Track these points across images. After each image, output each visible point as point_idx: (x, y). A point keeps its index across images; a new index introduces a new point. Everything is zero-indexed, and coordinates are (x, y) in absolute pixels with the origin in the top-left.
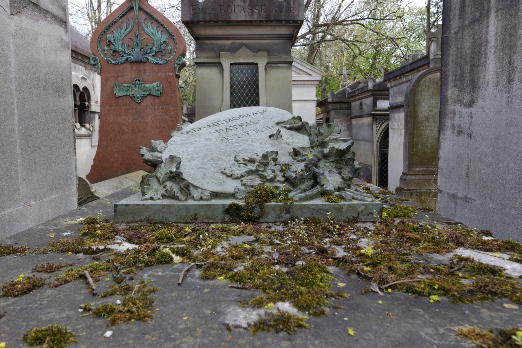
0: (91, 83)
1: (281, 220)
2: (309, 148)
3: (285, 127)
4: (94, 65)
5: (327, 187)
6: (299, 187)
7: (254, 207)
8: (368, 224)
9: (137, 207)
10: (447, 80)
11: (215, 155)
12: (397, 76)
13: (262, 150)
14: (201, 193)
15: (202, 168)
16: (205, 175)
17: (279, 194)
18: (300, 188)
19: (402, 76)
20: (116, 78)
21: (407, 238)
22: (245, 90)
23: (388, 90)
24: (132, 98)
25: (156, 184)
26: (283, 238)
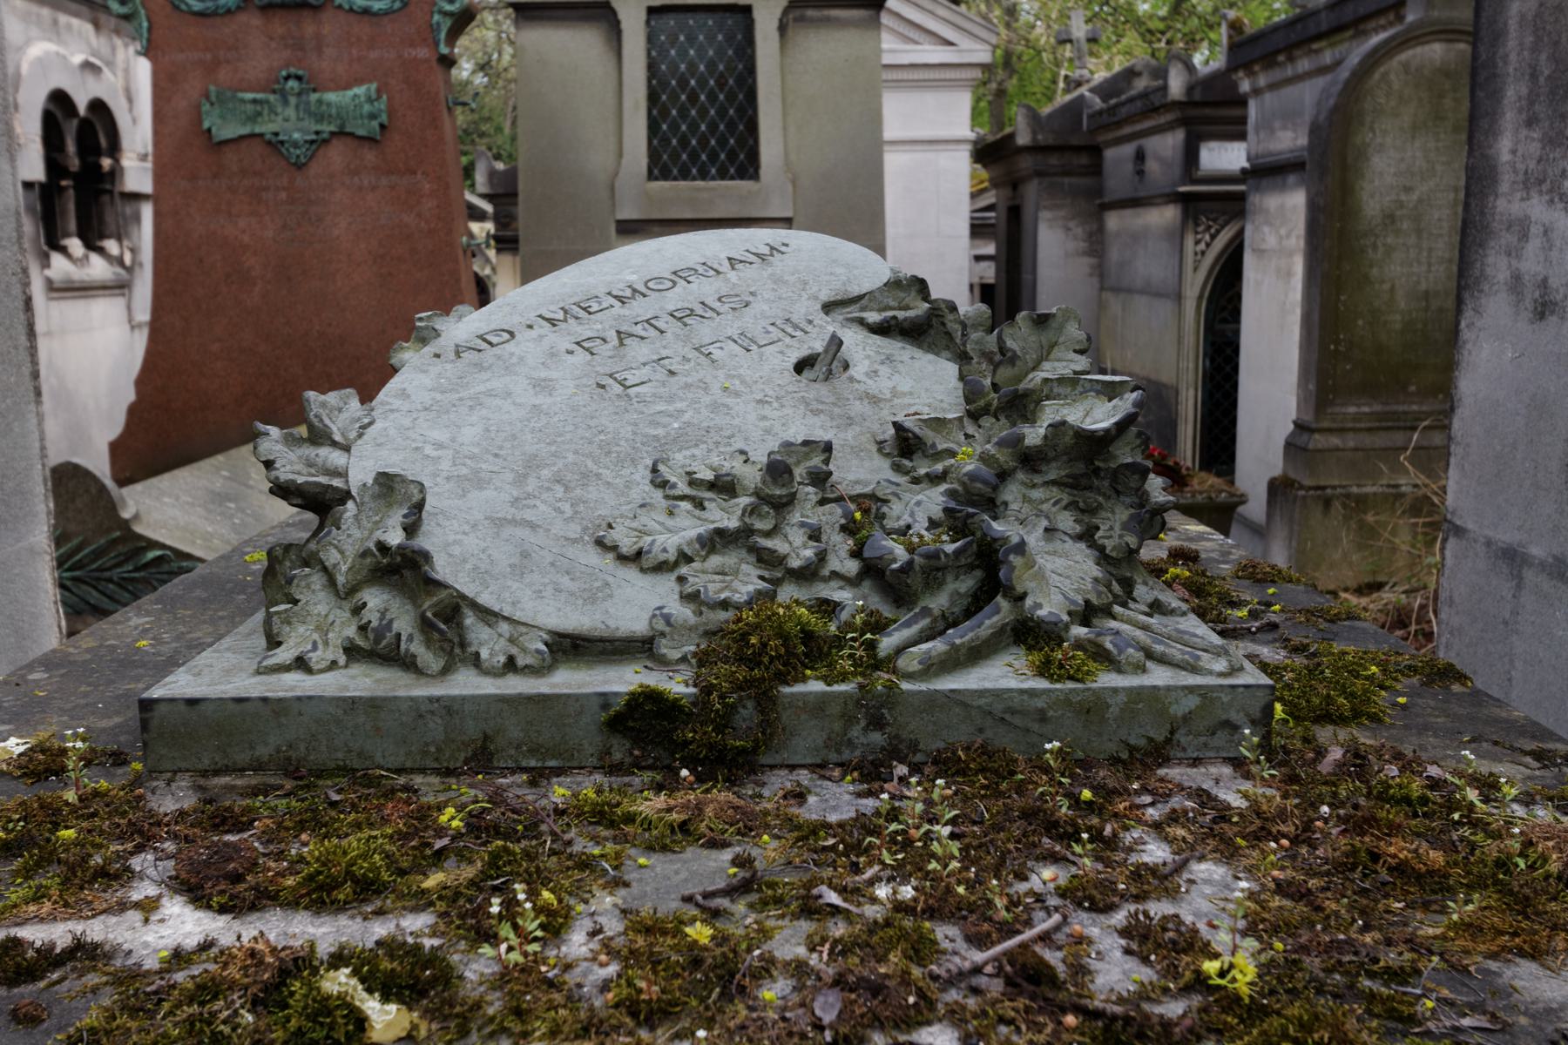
0: (120, 83)
1: (846, 755)
2: (960, 419)
3: (861, 322)
4: (126, 18)
5: (1039, 606)
6: (922, 604)
7: (733, 707)
8: (1213, 770)
9: (231, 706)
10: (1496, 95)
11: (571, 457)
12: (1278, 52)
13: (768, 431)
14: (511, 640)
15: (514, 522)
16: (525, 555)
17: (838, 642)
18: (926, 611)
19: (1297, 53)
20: (211, 68)
21: (1391, 869)
22: (703, 112)
23: (1242, 102)
24: (274, 145)
25: (322, 595)
26: (856, 869)
